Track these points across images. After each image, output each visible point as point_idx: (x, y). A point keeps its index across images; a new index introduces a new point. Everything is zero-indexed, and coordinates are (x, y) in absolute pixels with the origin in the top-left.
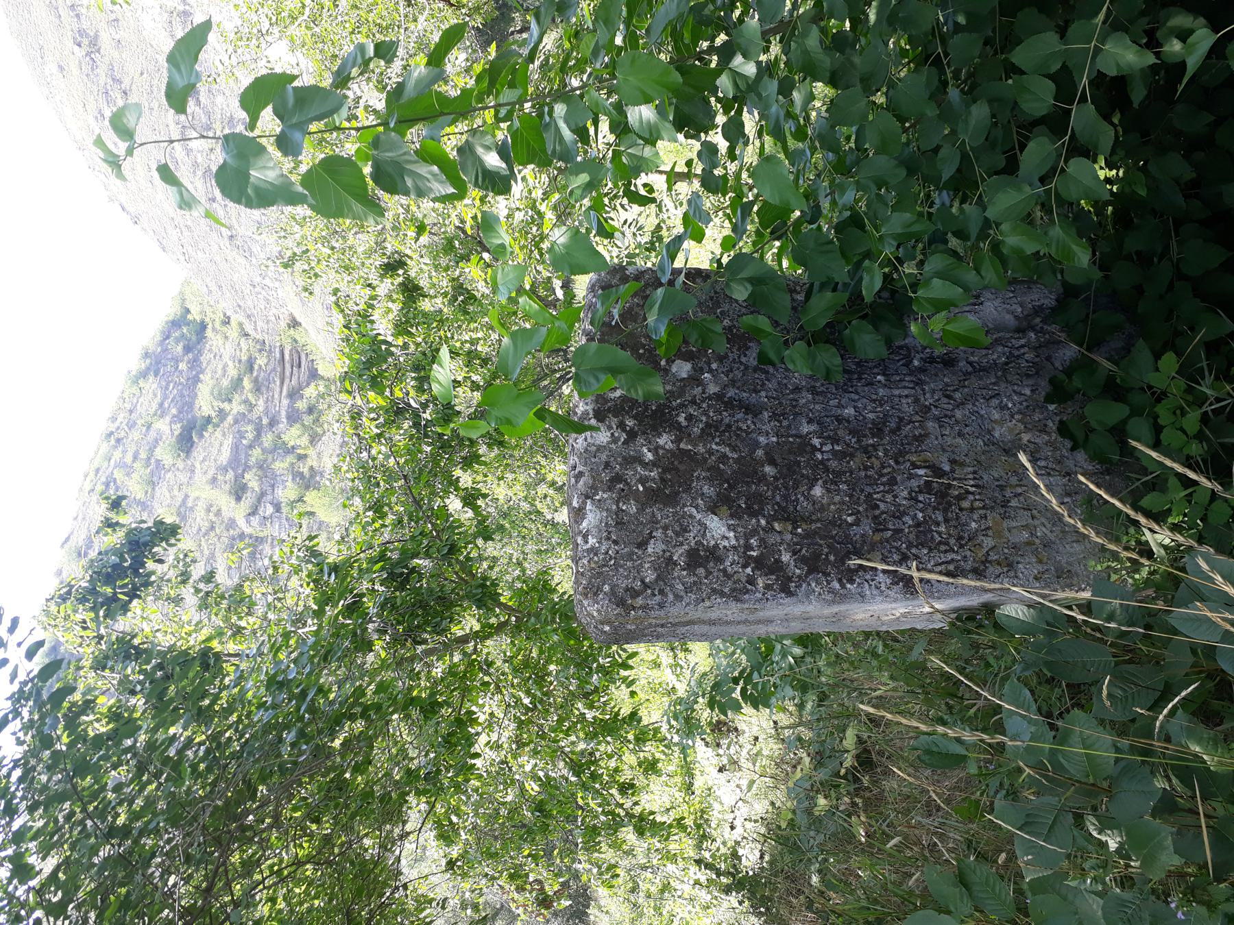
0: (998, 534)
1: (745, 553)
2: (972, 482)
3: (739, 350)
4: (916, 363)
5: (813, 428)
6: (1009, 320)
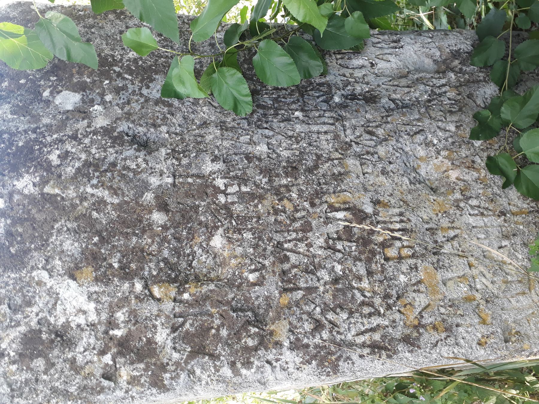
0: (433, 290)
1: (106, 332)
2: (398, 226)
3: (141, 81)
4: (337, 99)
5: (219, 166)
6: (428, 63)
